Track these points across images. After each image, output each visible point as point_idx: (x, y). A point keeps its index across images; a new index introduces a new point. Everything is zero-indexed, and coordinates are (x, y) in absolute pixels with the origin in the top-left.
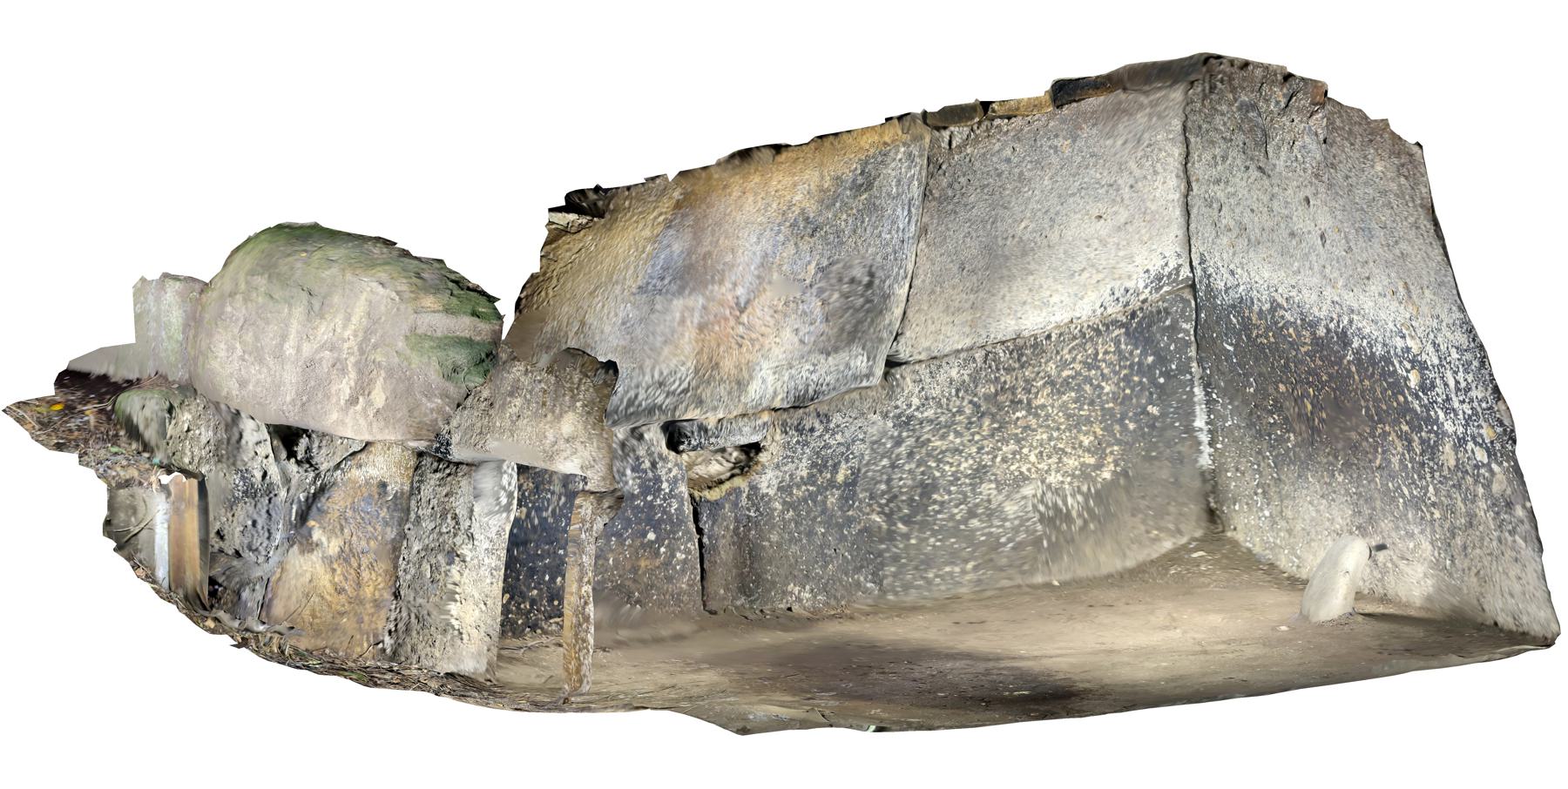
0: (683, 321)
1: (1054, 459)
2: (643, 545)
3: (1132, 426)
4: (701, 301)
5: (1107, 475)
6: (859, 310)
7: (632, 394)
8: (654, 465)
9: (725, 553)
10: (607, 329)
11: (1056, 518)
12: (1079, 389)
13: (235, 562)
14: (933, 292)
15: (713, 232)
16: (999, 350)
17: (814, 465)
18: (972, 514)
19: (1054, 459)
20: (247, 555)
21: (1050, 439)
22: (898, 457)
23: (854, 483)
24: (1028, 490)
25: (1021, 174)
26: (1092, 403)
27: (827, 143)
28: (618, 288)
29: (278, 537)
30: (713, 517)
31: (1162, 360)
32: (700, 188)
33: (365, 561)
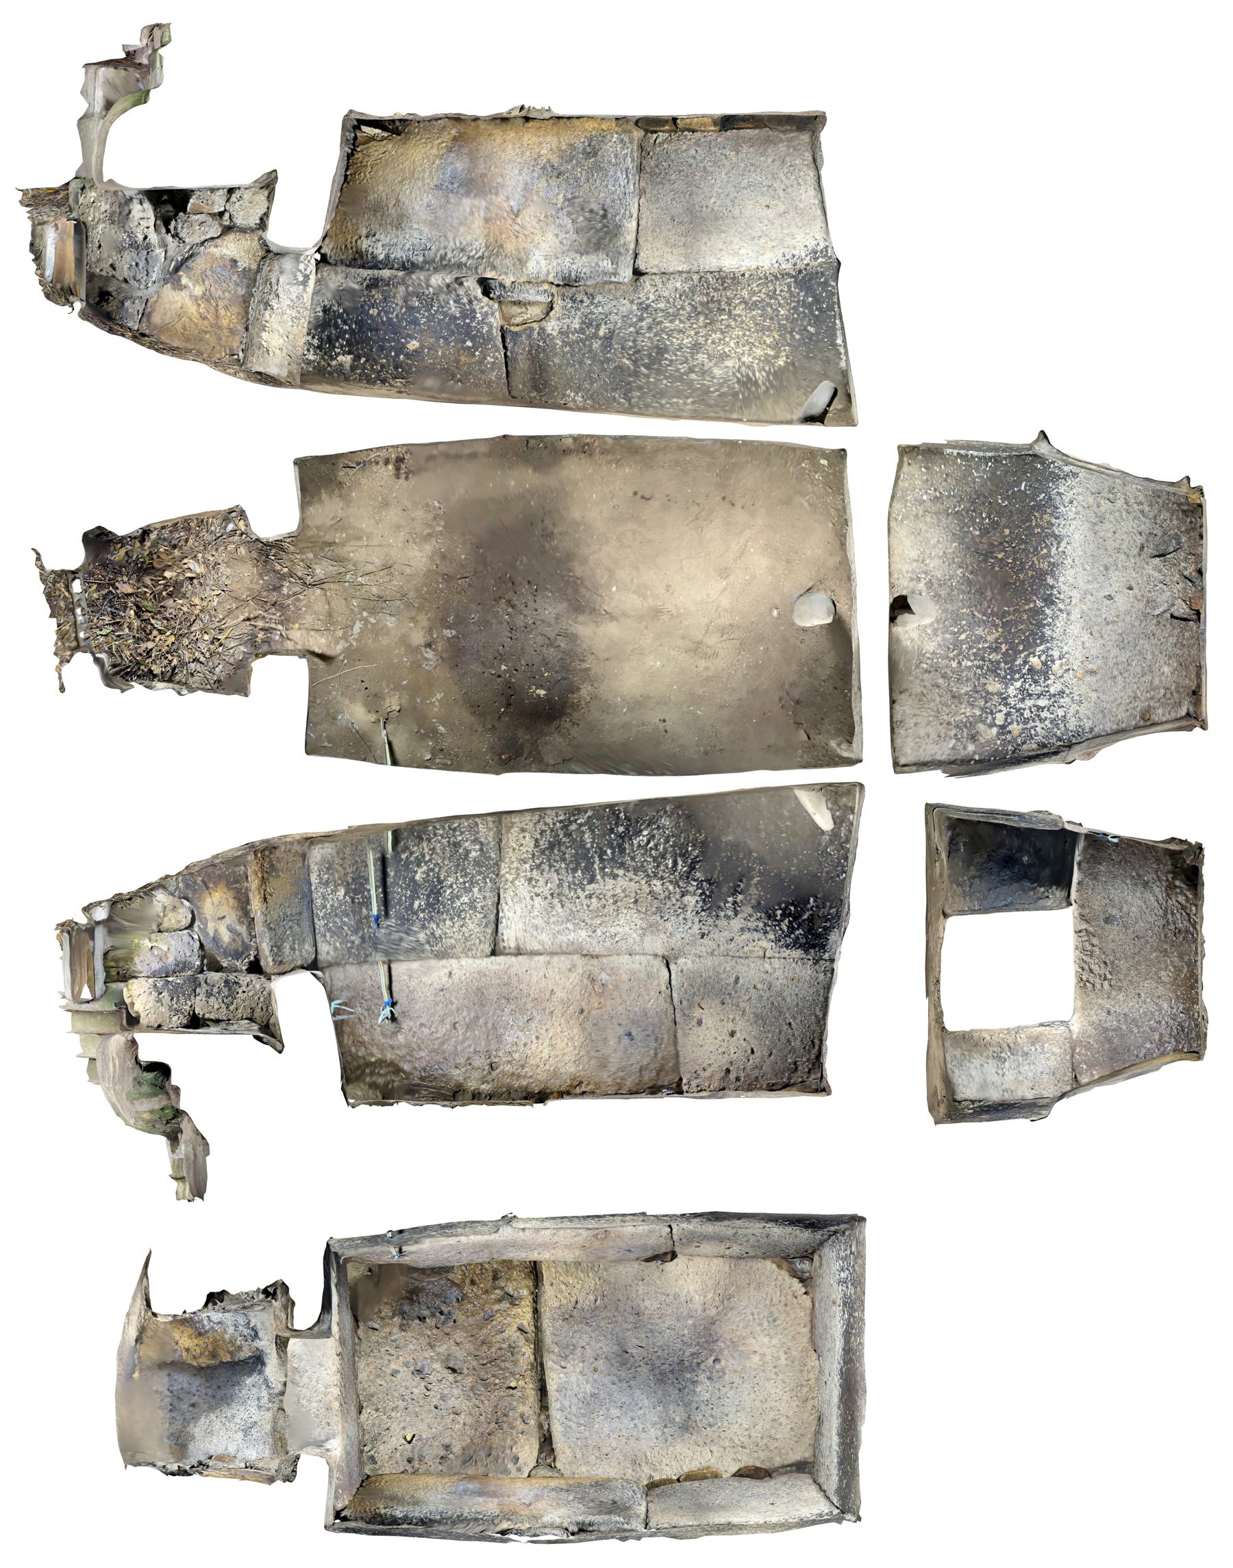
0: (472, 213)
1: (747, 348)
2: (463, 348)
3: (797, 337)
4: (484, 203)
5: (781, 363)
6: (600, 231)
7: (442, 252)
8: (470, 302)
9: (522, 364)
10: (417, 208)
11: (748, 383)
12: (763, 309)
13: (124, 285)
14: (654, 231)
15: (485, 162)
16: (709, 276)
17: (583, 323)
18: (691, 370)
19: (747, 348)
20: (132, 282)
21: (744, 335)
22: (641, 328)
23: (611, 338)
24: (729, 363)
25: (705, 168)
26: (772, 319)
27: (562, 122)
28: (420, 183)
29: (154, 276)
30: (514, 341)
31: (817, 300)
32: (470, 131)
33: (221, 304)
